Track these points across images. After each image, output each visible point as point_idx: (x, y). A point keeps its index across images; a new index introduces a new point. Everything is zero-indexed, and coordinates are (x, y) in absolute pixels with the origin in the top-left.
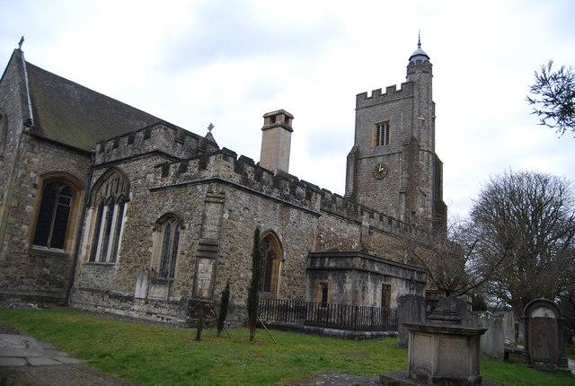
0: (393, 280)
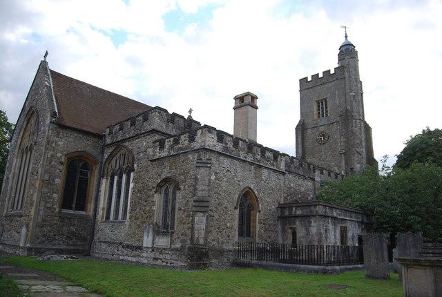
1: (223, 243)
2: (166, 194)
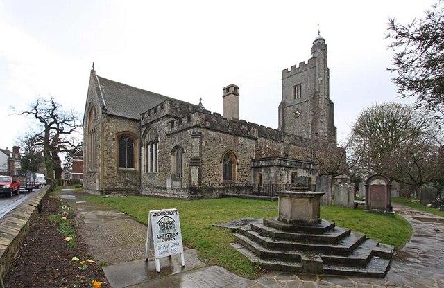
0: (298, 170)
1: (212, 184)
2: (178, 156)
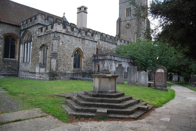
1: (66, 70)
2: (44, 51)
